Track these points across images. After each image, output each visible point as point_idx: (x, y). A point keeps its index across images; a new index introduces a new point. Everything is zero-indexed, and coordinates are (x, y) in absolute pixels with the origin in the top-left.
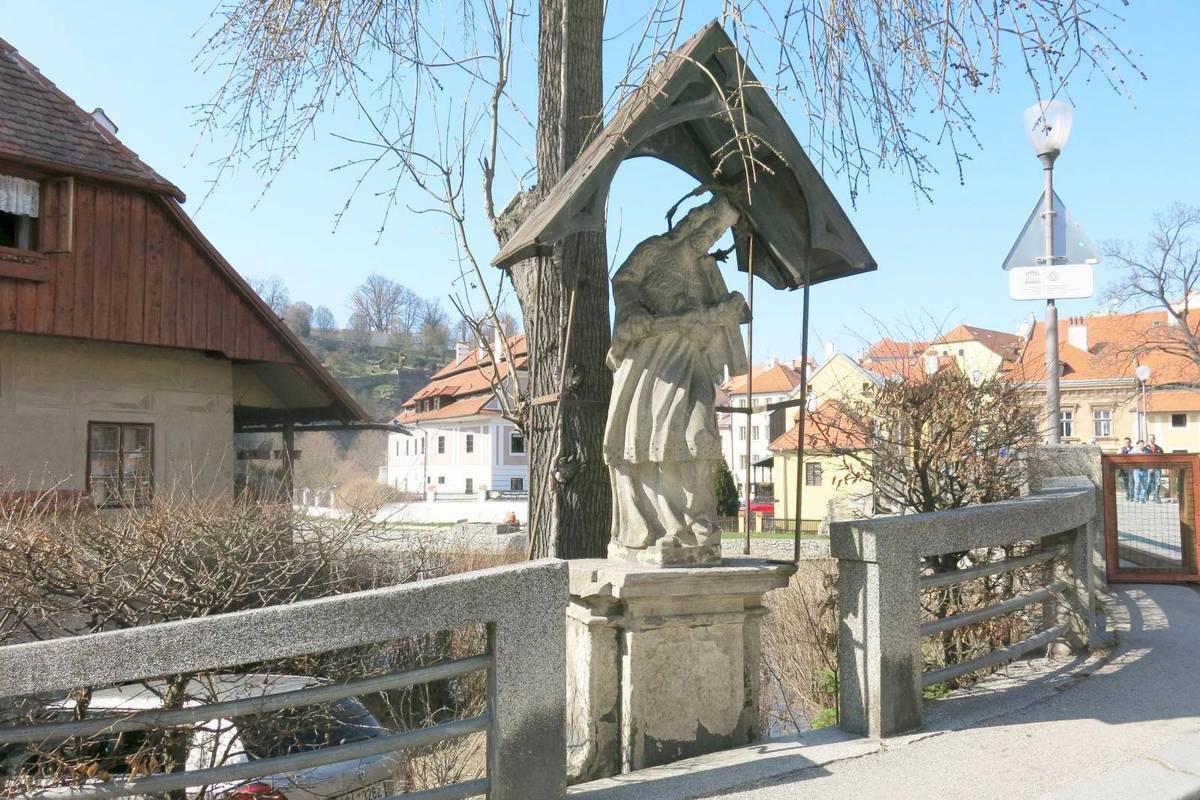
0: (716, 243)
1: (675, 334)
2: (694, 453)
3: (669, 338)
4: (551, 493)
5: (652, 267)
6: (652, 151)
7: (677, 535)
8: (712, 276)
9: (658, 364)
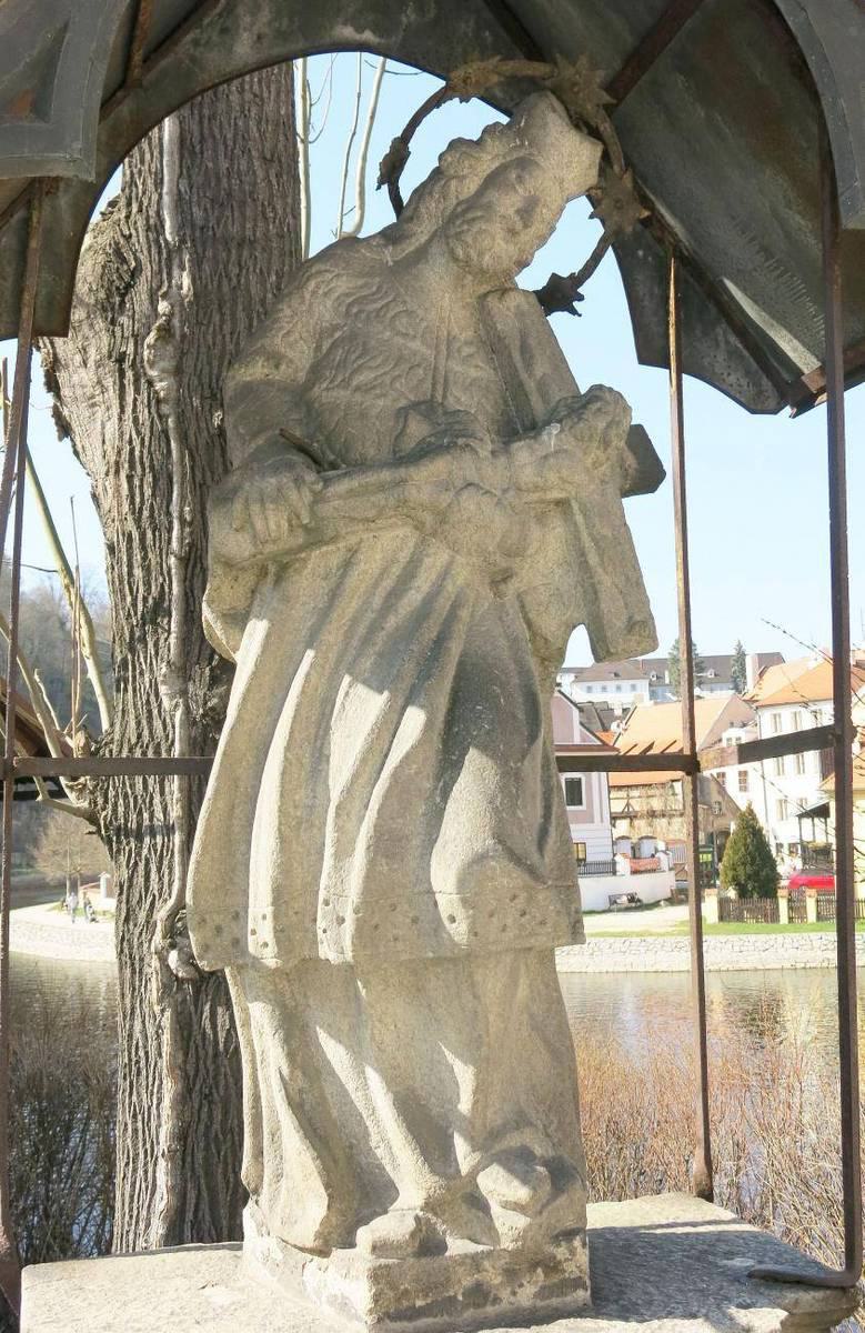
0: (541, 257)
1: (400, 532)
2: (459, 931)
3: (385, 546)
4: (157, 1009)
5: (335, 328)
6: (368, 36)
7: (429, 1206)
8: (524, 348)
9: (349, 635)
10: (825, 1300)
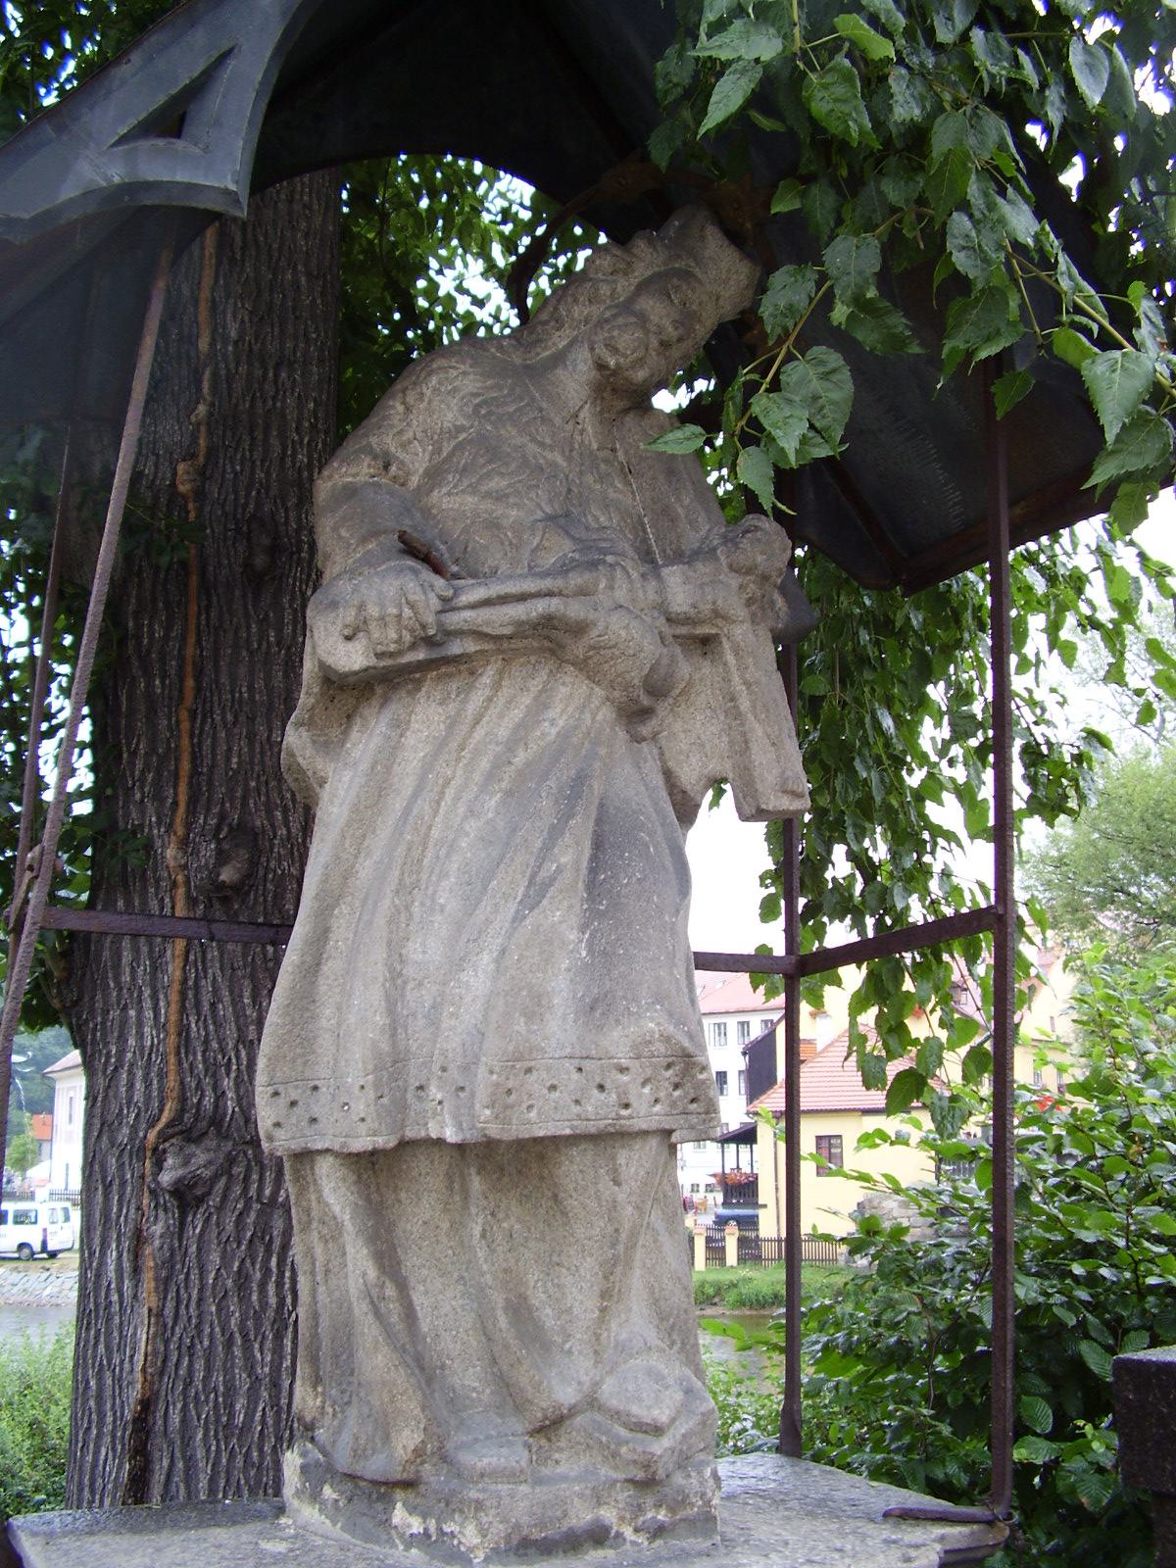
5: (460, 429)
10: (973, 1533)
